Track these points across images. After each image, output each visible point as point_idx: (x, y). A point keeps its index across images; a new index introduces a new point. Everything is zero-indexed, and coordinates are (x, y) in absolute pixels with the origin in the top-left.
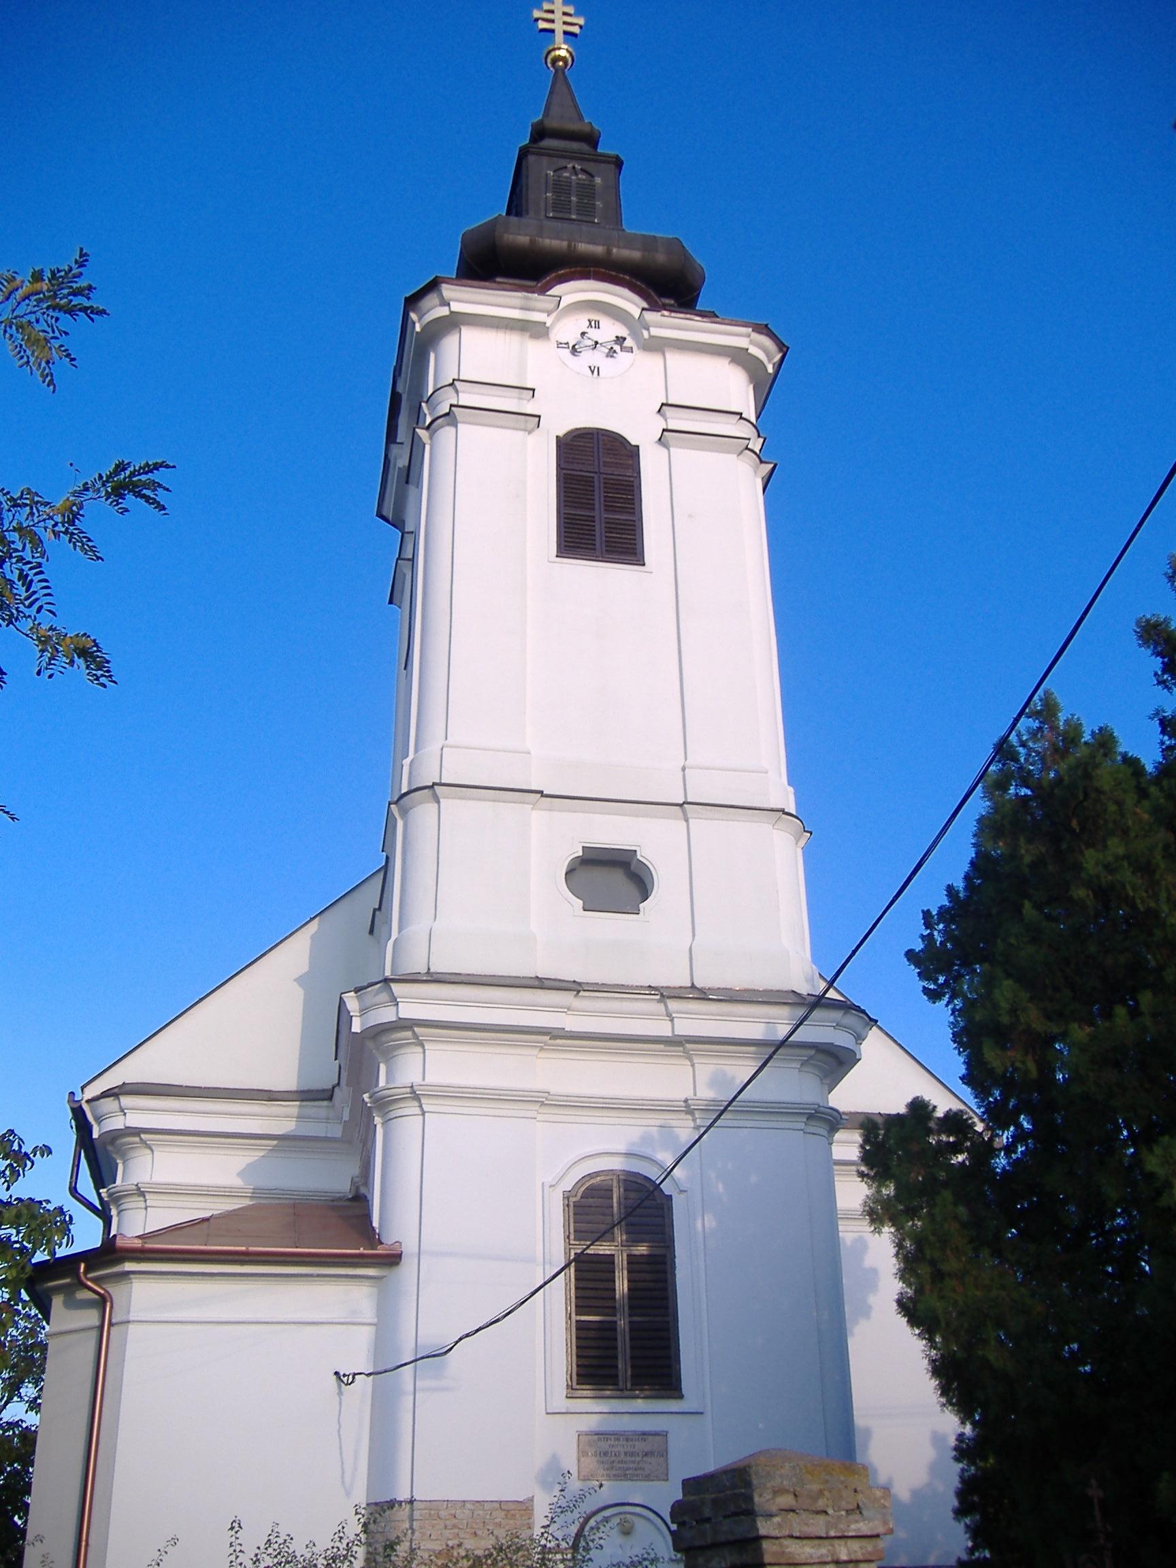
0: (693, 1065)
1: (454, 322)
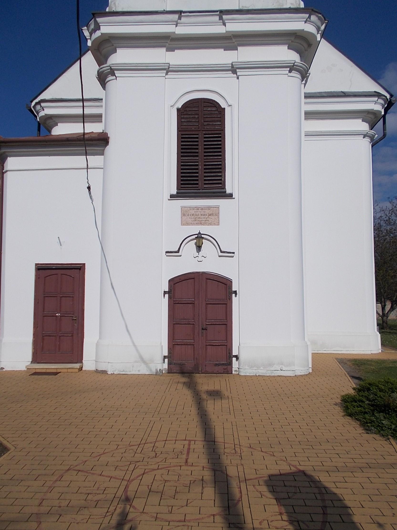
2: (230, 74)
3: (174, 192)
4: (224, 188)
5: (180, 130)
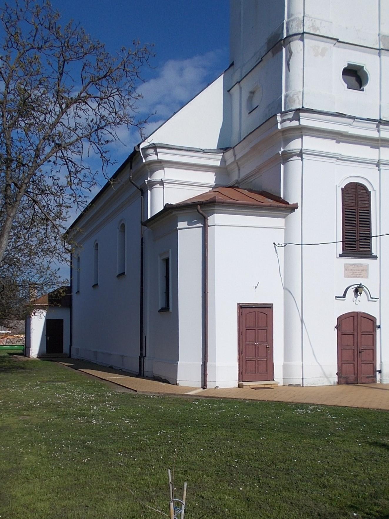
2: (374, 167)
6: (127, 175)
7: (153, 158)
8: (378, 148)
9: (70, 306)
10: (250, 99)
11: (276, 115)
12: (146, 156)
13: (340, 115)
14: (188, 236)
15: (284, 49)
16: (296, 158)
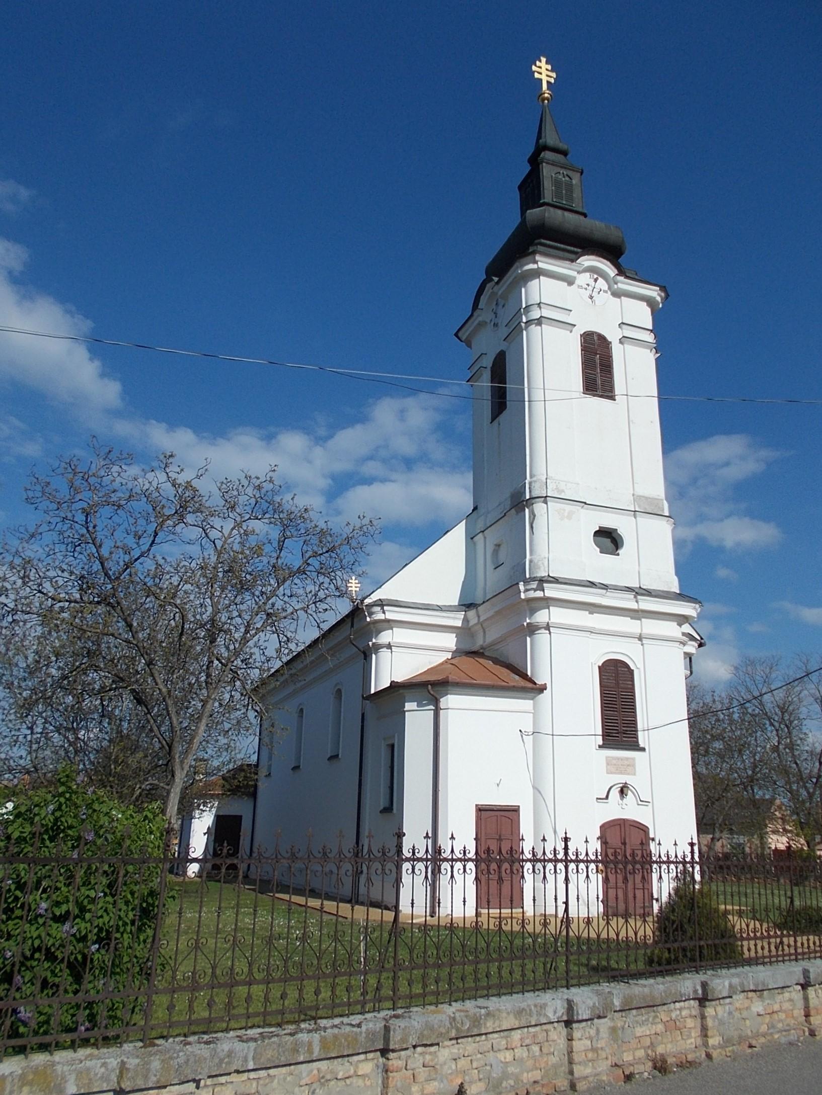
0: (550, 633)
1: (538, 273)
3: (601, 743)
4: (637, 742)
5: (697, 777)
6: (345, 631)
7: (380, 616)
8: (640, 619)
9: (254, 795)
10: (496, 552)
11: (518, 584)
12: (371, 614)
13: (592, 584)
14: (416, 720)
15: (527, 510)
16: (543, 631)
